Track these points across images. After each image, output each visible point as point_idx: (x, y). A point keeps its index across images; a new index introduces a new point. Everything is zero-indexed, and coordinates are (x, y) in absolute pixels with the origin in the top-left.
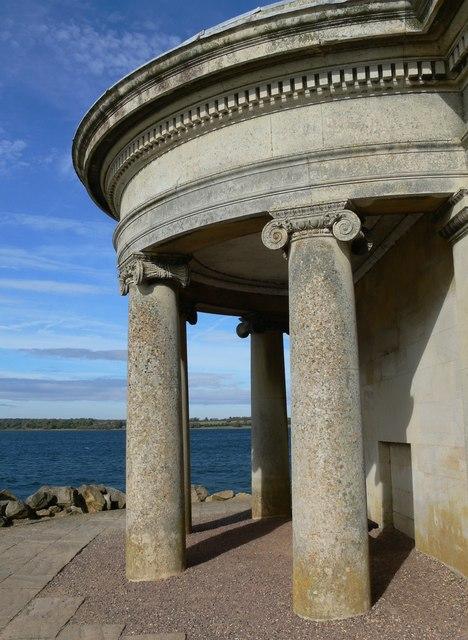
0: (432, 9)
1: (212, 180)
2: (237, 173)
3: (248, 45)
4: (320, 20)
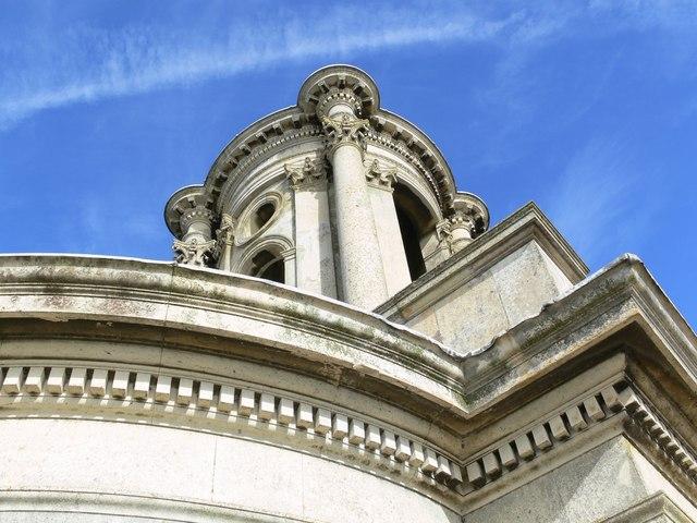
0: (661, 308)
1: (77, 502)
2: (142, 506)
3: (247, 315)
4: (364, 336)
